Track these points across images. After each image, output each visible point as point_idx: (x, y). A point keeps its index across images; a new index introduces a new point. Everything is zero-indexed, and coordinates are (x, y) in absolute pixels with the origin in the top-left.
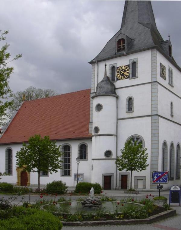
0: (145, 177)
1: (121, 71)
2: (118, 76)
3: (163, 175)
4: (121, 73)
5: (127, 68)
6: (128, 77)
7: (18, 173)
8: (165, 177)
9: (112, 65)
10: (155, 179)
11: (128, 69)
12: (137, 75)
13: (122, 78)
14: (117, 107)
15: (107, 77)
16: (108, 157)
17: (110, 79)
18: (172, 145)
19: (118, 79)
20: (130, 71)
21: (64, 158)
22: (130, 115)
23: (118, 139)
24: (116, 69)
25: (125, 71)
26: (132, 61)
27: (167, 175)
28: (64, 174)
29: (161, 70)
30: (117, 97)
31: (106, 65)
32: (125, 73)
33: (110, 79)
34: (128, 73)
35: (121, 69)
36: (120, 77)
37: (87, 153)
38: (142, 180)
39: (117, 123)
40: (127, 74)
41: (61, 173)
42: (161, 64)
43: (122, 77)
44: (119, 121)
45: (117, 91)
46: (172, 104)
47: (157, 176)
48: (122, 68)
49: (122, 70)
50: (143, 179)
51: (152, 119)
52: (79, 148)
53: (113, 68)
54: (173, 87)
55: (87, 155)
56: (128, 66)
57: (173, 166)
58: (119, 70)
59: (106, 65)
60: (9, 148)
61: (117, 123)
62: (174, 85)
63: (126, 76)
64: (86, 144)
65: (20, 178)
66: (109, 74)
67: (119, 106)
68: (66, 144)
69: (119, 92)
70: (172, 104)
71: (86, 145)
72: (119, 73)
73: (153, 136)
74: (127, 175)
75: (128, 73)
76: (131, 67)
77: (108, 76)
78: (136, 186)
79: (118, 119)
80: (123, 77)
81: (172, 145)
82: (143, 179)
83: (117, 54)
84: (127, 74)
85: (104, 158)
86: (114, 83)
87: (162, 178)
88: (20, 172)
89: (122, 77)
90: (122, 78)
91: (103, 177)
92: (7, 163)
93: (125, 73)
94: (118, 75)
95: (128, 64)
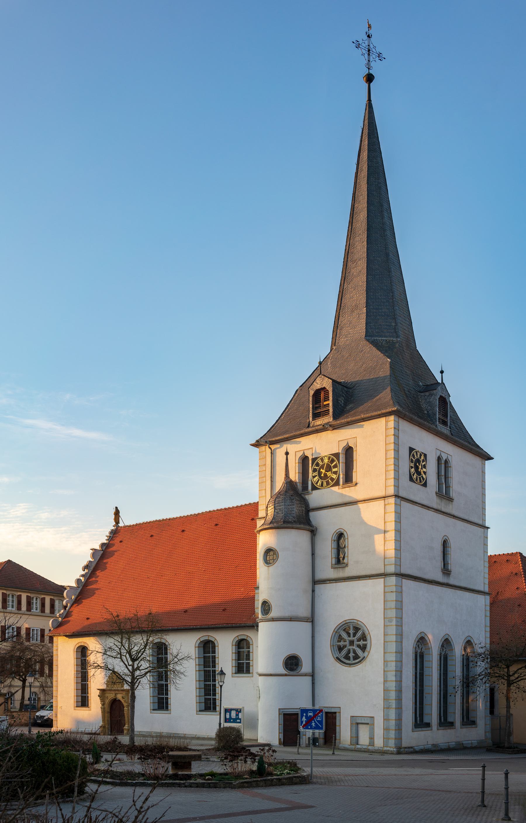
0: (373, 717)
1: (319, 470)
2: (315, 479)
3: (315, 716)
4: (320, 473)
5: (333, 461)
6: (337, 484)
7: (103, 705)
8: (319, 719)
9: (301, 453)
10: (304, 723)
11: (335, 463)
12: (354, 480)
13: (322, 485)
14: (313, 554)
15: (291, 481)
16: (291, 670)
17: (300, 487)
18: (446, 643)
19: (314, 488)
20: (341, 469)
21: (82, 696)
22: (341, 574)
23: (317, 629)
24: (310, 462)
25: (329, 469)
26: (344, 444)
27: (322, 715)
28: (157, 708)
29: (412, 465)
30: (313, 532)
31: (287, 454)
32: (329, 474)
33: (300, 487)
34: (335, 473)
35: (321, 463)
36: (320, 483)
37: (251, 659)
38: (368, 726)
39: (313, 591)
40: (334, 476)
41: (152, 704)
42: (411, 449)
43: (322, 483)
44: (317, 587)
45: (312, 514)
46: (445, 544)
47: (307, 717)
48: (322, 460)
49: (322, 467)
50: (368, 724)
51: (386, 585)
52: (234, 647)
53: (304, 460)
54: (451, 500)
55: (251, 664)
56: (337, 455)
57: (429, 694)
58: (317, 464)
59: (287, 454)
60: (82, 644)
61: (313, 591)
62: (453, 494)
63: (332, 479)
64: (248, 639)
65: (107, 715)
66: (295, 476)
67: (318, 552)
68: (207, 638)
69: (316, 517)
70: (445, 544)
71: (250, 641)
72: (316, 473)
73: (389, 624)
74: (335, 713)
75: (335, 473)
76: (342, 458)
77: (293, 480)
78: (355, 738)
79: (315, 582)
80: (325, 483)
81: (446, 643)
82: (368, 724)
83: (311, 425)
84: (334, 476)
85: (283, 671)
86: (307, 497)
87: (314, 722)
88: (107, 701)
89: (322, 483)
90: (322, 485)
91: (282, 717)
92: (80, 680)
93: (329, 474)
94: (314, 477)
95: (335, 451)
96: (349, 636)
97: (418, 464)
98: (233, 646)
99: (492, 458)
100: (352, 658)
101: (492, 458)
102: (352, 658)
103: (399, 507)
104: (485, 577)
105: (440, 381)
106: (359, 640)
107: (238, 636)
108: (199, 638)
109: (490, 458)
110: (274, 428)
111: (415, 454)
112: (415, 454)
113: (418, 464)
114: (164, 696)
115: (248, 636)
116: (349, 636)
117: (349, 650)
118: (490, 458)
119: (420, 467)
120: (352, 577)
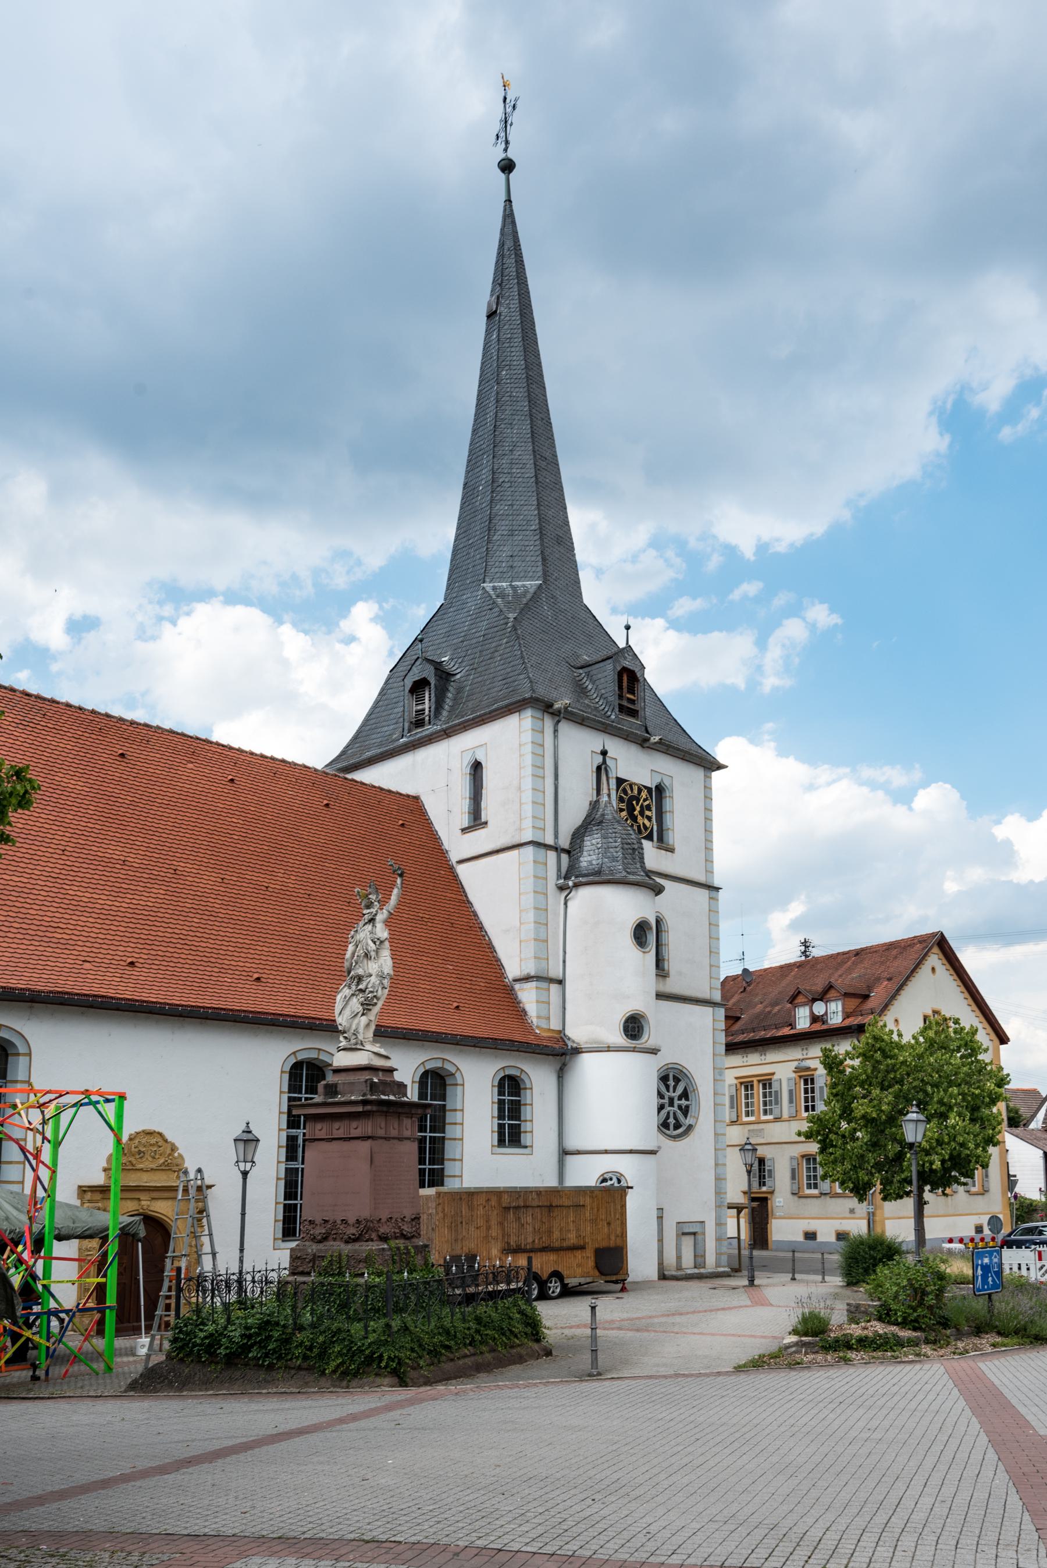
37: (281, 1208)
96: (668, 1091)
97: (634, 802)
98: (281, 1132)
99: (727, 767)
100: (671, 1127)
101: (727, 767)
102: (671, 1127)
103: (713, 976)
104: (542, 794)
105: (622, 644)
106: (680, 1098)
107: (503, 1068)
108: (423, 1063)
109: (720, 767)
110: (762, 1034)
111: (628, 789)
112: (628, 789)
113: (634, 802)
114: (507, 1122)
115: (522, 1070)
116: (668, 1091)
117: (668, 1113)
118: (720, 767)
119: (638, 808)
120: (813, 1038)
